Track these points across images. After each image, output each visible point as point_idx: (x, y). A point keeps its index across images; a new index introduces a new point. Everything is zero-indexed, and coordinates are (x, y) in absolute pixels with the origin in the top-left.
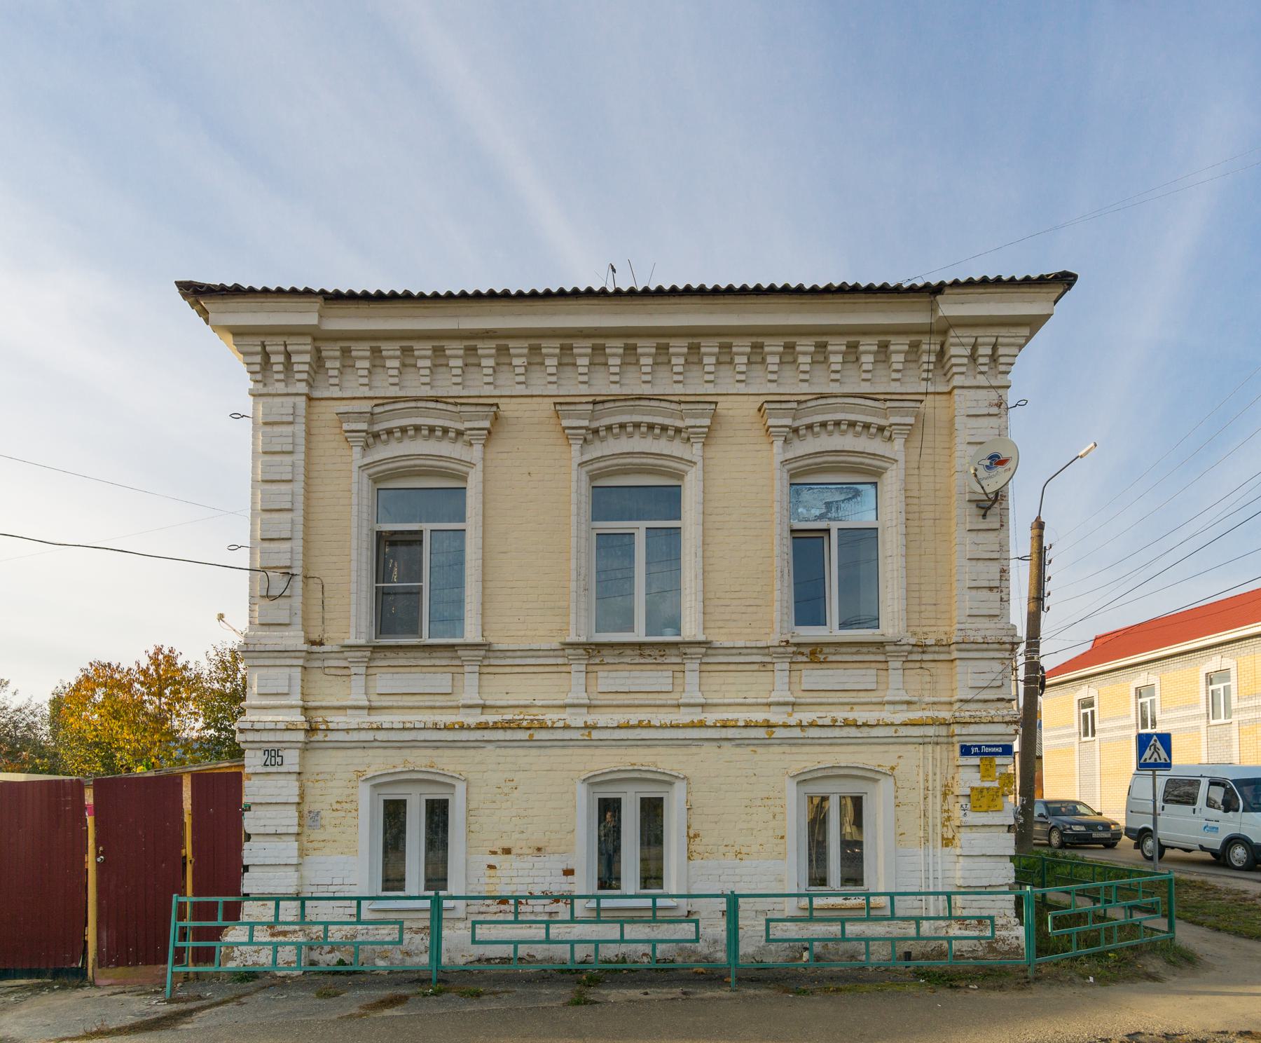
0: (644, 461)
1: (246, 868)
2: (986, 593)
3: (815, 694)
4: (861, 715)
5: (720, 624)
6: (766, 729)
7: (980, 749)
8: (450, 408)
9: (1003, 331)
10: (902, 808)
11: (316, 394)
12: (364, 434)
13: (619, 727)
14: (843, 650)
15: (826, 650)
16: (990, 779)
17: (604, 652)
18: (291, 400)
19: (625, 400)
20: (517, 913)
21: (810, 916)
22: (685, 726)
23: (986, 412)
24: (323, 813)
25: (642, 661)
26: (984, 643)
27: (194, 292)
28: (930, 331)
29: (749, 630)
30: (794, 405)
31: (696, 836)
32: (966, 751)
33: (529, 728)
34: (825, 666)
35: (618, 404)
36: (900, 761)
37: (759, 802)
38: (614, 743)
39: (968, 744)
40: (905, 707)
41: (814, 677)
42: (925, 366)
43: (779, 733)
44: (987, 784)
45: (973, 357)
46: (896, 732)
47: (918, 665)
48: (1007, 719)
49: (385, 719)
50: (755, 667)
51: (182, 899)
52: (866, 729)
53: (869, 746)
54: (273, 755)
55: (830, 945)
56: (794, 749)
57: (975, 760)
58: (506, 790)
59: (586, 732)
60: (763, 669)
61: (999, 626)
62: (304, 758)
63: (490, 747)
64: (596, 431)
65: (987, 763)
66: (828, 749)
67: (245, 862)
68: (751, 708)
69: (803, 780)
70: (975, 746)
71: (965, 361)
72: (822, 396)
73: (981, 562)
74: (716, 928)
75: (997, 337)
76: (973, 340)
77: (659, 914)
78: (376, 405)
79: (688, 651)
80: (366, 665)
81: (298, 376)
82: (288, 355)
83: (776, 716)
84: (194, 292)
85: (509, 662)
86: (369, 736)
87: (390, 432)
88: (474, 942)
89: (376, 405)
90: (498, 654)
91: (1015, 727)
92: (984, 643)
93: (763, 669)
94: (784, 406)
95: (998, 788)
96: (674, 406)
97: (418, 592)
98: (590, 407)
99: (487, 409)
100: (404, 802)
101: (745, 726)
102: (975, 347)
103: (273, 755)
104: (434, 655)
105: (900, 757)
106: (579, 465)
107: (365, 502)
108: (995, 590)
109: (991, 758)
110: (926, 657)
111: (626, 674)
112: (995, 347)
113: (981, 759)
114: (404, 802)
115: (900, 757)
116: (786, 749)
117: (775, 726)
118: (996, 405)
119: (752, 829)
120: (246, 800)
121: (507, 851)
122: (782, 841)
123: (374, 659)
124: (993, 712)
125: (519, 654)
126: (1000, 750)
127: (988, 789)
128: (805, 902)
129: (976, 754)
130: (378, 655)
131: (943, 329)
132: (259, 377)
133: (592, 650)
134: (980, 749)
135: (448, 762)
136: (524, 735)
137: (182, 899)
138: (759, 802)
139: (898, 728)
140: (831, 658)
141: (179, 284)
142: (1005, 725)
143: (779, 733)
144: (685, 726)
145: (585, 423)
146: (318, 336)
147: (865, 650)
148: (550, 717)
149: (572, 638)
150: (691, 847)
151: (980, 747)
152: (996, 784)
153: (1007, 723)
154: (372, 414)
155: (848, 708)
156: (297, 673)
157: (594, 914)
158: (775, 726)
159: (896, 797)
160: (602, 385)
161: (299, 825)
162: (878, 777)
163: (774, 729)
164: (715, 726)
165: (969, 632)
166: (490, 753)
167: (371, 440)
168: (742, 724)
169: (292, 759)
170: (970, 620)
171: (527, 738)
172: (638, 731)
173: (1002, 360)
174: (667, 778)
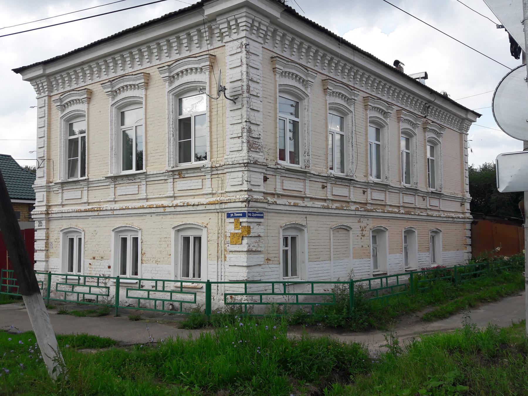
0: (126, 101)
1: (36, 262)
2: (237, 140)
3: (182, 192)
4: (192, 201)
5: (152, 164)
6: (163, 208)
7: (234, 215)
8: (77, 92)
9: (235, 13)
10: (210, 242)
11: (52, 94)
12: (168, 78)
13: (120, 209)
14: (189, 172)
15: (183, 172)
16: (237, 229)
17: (118, 179)
18: (43, 99)
19: (120, 78)
20: (98, 282)
21: (181, 290)
22: (138, 208)
23: (236, 52)
24: (53, 243)
25: (129, 182)
26: (232, 164)
27: (17, 71)
28: (204, 23)
29: (160, 166)
30: (167, 67)
31: (144, 253)
32: (229, 216)
33: (98, 211)
34: (185, 179)
35: (118, 80)
36: (210, 220)
37: (163, 240)
38: (121, 215)
39: (230, 212)
40: (211, 196)
41: (181, 184)
42: (205, 39)
43: (168, 210)
44: (237, 231)
45: (229, 27)
46: (205, 207)
47: (217, 176)
48: (241, 200)
49: (65, 209)
50: (163, 181)
51: (5, 271)
52: (195, 207)
53: (199, 214)
54: (40, 222)
55: (142, 301)
56: (175, 216)
57: (232, 220)
58: (94, 235)
59: (112, 211)
60: (165, 182)
61: (241, 155)
62: (49, 224)
63: (90, 218)
64: (173, 77)
65: (237, 221)
66: (185, 216)
67: (35, 259)
68: (162, 199)
69: (178, 230)
70: (232, 213)
71: (226, 29)
72: (177, 61)
73: (235, 125)
74: (201, 298)
75: (227, 18)
76: (226, 20)
77: (183, 290)
78: (61, 96)
79: (140, 177)
80: (210, 174)
81: (241, 28)
82: (236, 20)
83: (165, 203)
84: (17, 71)
85: (95, 185)
86: (60, 215)
87: (178, 74)
88: (127, 297)
89: (61, 96)
90: (91, 182)
91: (245, 203)
92: (232, 164)
93: (165, 182)
94: (164, 68)
95: (241, 233)
96: (133, 77)
97: (77, 160)
98: (109, 83)
99: (84, 91)
100: (126, 238)
101: (157, 207)
102: (229, 22)
103: (40, 222)
104: (76, 184)
105: (210, 219)
106: (111, 105)
107: (63, 130)
108: (241, 138)
109: (238, 219)
110: (219, 172)
111: (124, 187)
112: (236, 20)
113: (235, 219)
114: (126, 238)
115: (210, 219)
116: (172, 216)
117: (166, 207)
118: (240, 47)
119: (161, 251)
120: (35, 238)
121: (94, 258)
122: (169, 256)
123: (213, 171)
124: (238, 197)
125: (96, 182)
126: (241, 215)
127: (236, 233)
128: (179, 284)
129: (232, 217)
130: (64, 186)
131: (213, 18)
132: (38, 92)
133: (115, 179)
134: (234, 215)
135: (135, 223)
136: (96, 213)
137: (5, 271)
138: (163, 240)
139: (206, 205)
140: (186, 176)
141: (12, 70)
142: (241, 203)
143: (168, 210)
144: (138, 208)
145: (110, 90)
146: (273, 21)
147: (196, 171)
148: (104, 206)
149: (110, 175)
150: (143, 258)
151: (234, 213)
152: (240, 231)
153: (242, 202)
154: (61, 99)
155: (193, 197)
156: (45, 193)
157: (65, 281)
158: (166, 207)
159: (208, 237)
160: (112, 75)
161: (46, 247)
162: (202, 228)
163: (166, 208)
164: (147, 208)
165: (229, 160)
166: (90, 220)
167: (172, 79)
168: (155, 206)
169: (44, 223)
170: (231, 153)
171: (97, 214)
172: (126, 211)
173: (240, 25)
174: (136, 230)
